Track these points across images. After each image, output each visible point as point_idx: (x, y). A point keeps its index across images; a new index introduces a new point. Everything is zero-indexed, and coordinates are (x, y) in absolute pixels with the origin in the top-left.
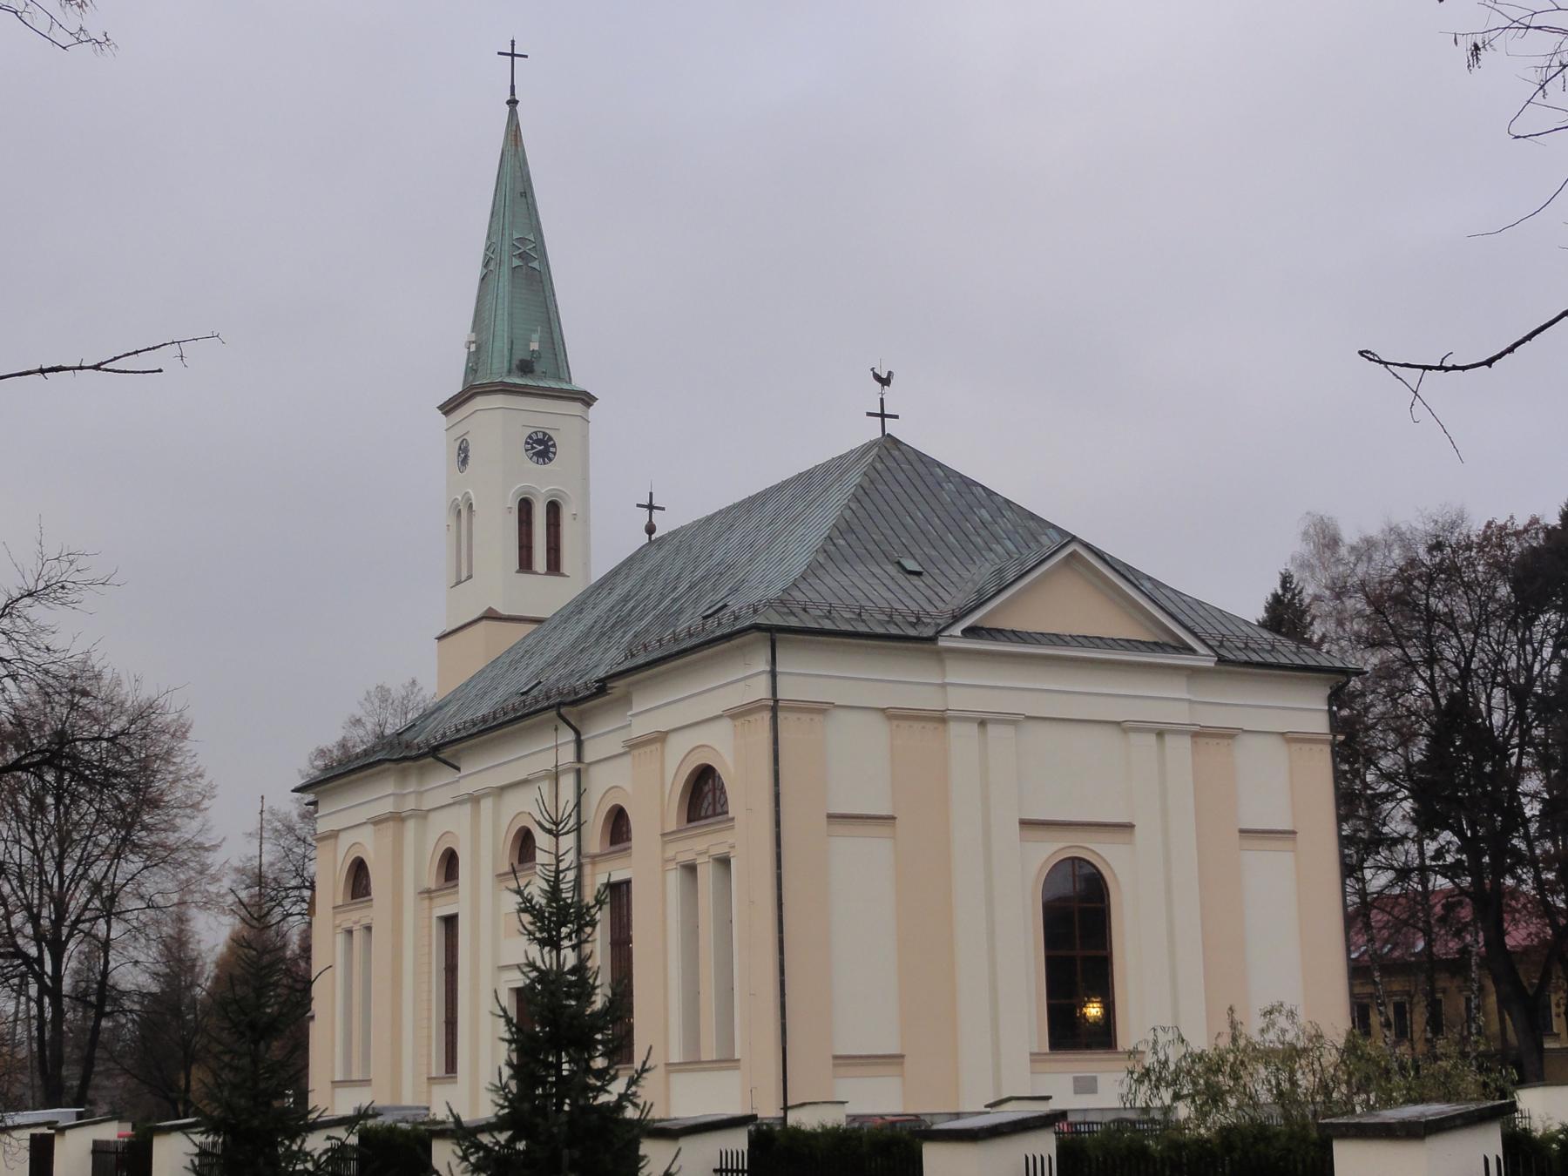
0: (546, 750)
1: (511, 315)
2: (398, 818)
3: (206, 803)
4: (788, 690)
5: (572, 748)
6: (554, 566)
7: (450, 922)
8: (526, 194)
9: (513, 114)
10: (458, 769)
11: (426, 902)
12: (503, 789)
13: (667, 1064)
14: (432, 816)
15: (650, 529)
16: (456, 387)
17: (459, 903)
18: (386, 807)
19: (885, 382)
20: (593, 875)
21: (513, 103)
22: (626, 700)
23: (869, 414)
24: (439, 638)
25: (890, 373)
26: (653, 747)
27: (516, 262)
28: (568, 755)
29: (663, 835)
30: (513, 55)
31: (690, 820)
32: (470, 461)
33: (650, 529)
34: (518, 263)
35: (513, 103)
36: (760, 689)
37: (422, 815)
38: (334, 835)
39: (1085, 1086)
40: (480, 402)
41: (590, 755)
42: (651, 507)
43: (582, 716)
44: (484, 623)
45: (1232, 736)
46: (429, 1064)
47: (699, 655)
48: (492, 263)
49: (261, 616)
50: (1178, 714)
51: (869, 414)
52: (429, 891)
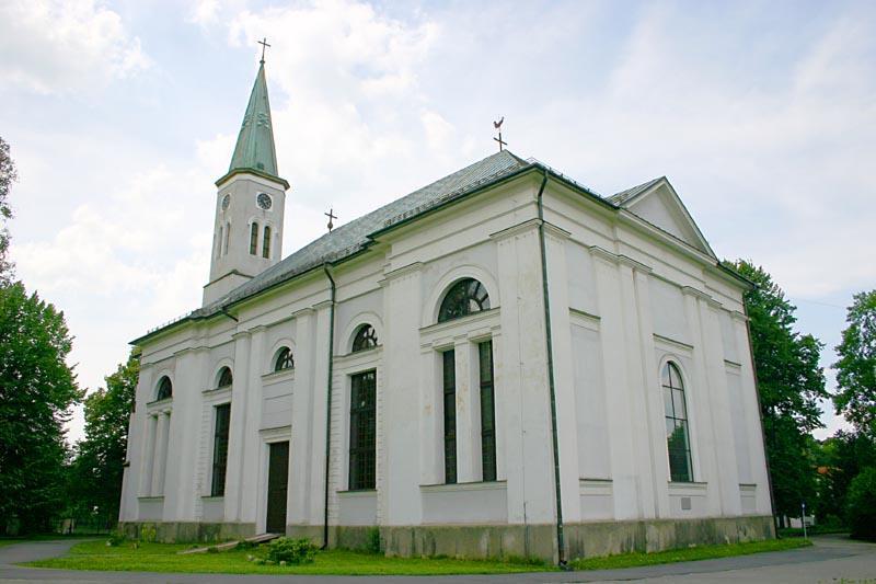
0: (319, 292)
7: (224, 411)
9: (262, 67)
15: (330, 226)
16: (225, 171)
21: (262, 62)
28: (328, 296)
33: (330, 226)
34: (258, 123)
35: (262, 62)
39: (686, 504)
42: (331, 216)
47: (459, 205)
49: (114, 279)
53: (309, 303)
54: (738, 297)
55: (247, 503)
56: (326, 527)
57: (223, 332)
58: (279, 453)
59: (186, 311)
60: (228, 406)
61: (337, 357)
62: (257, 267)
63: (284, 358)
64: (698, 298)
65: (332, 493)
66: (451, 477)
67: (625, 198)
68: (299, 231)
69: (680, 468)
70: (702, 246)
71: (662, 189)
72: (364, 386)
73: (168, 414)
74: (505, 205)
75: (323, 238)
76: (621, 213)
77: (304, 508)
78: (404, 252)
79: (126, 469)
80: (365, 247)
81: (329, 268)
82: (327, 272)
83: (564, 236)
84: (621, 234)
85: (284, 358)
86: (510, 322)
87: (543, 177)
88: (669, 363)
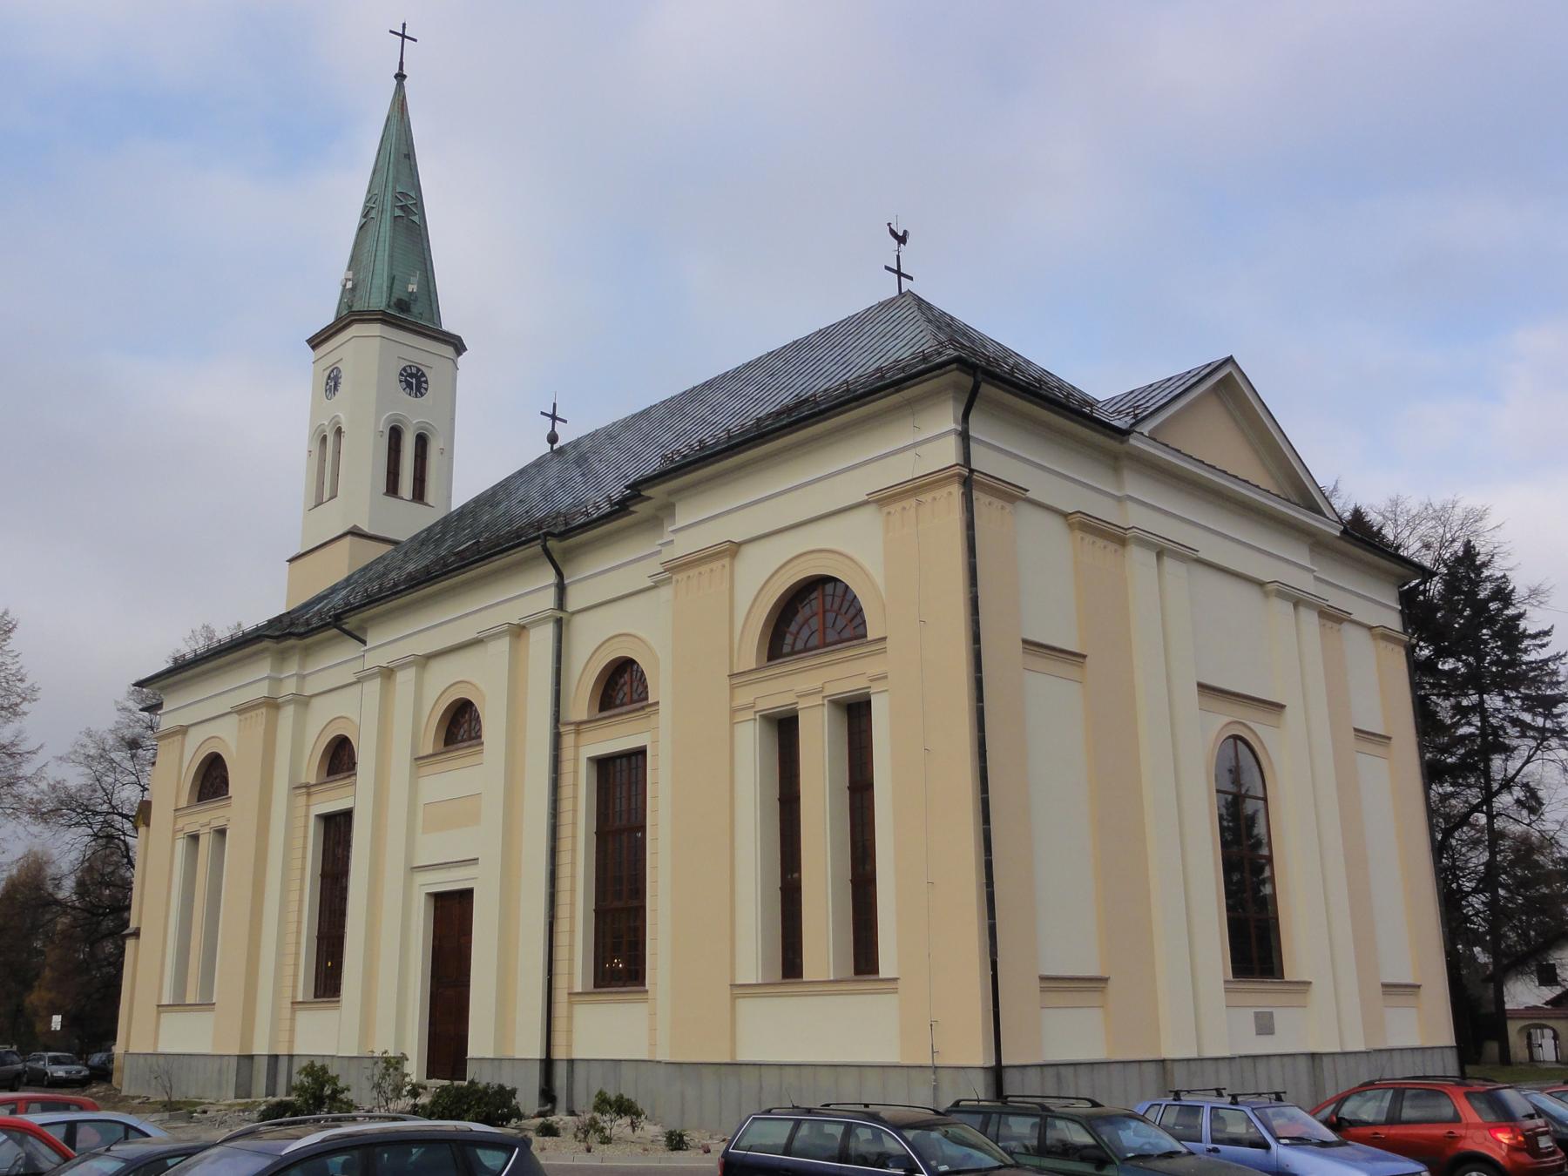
0: (526, 593)
1: (391, 256)
2: (272, 704)
3: (25, 707)
4: (983, 461)
5: (551, 594)
6: (419, 495)
7: (337, 828)
8: (409, 156)
10: (364, 643)
11: (302, 800)
12: (430, 657)
13: (733, 986)
14: (315, 702)
15: (553, 438)
17: (355, 796)
18: (262, 691)
19: (902, 239)
20: (577, 747)
21: (400, 77)
22: (668, 509)
23: (887, 268)
24: (290, 561)
25: (905, 232)
26: (716, 565)
27: (398, 212)
28: (548, 600)
29: (731, 676)
30: (403, 36)
31: (770, 659)
32: (341, 388)
33: (553, 438)
34: (397, 214)
35: (400, 77)
36: (947, 453)
37: (303, 702)
38: (183, 730)
39: (1265, 1026)
40: (355, 330)
41: (573, 603)
42: (554, 417)
43: (571, 554)
44: (349, 538)
45: (1340, 621)
46: (295, 987)
48: (373, 214)
50: (1303, 582)
51: (887, 268)
52: (308, 786)
53: (514, 614)
54: (1391, 599)
55: (381, 1015)
56: (548, 1064)
57: (335, 663)
58: (452, 914)
59: (255, 616)
60: (347, 815)
61: (653, 1045)
62: (407, 521)
63: (460, 723)
64: (1296, 605)
65: (561, 996)
66: (791, 965)
67: (1141, 407)
68: (482, 456)
69: (1255, 947)
70: (1305, 495)
71: (1225, 386)
72: (620, 778)
73: (221, 832)
74: (898, 435)
75: (539, 464)
76: (1133, 441)
77: (500, 1035)
78: (701, 520)
79: (130, 944)
80: (621, 507)
81: (551, 543)
82: (548, 553)
83: (1011, 494)
84: (1135, 485)
85: (460, 723)
86: (911, 672)
87: (980, 377)
88: (1236, 738)
